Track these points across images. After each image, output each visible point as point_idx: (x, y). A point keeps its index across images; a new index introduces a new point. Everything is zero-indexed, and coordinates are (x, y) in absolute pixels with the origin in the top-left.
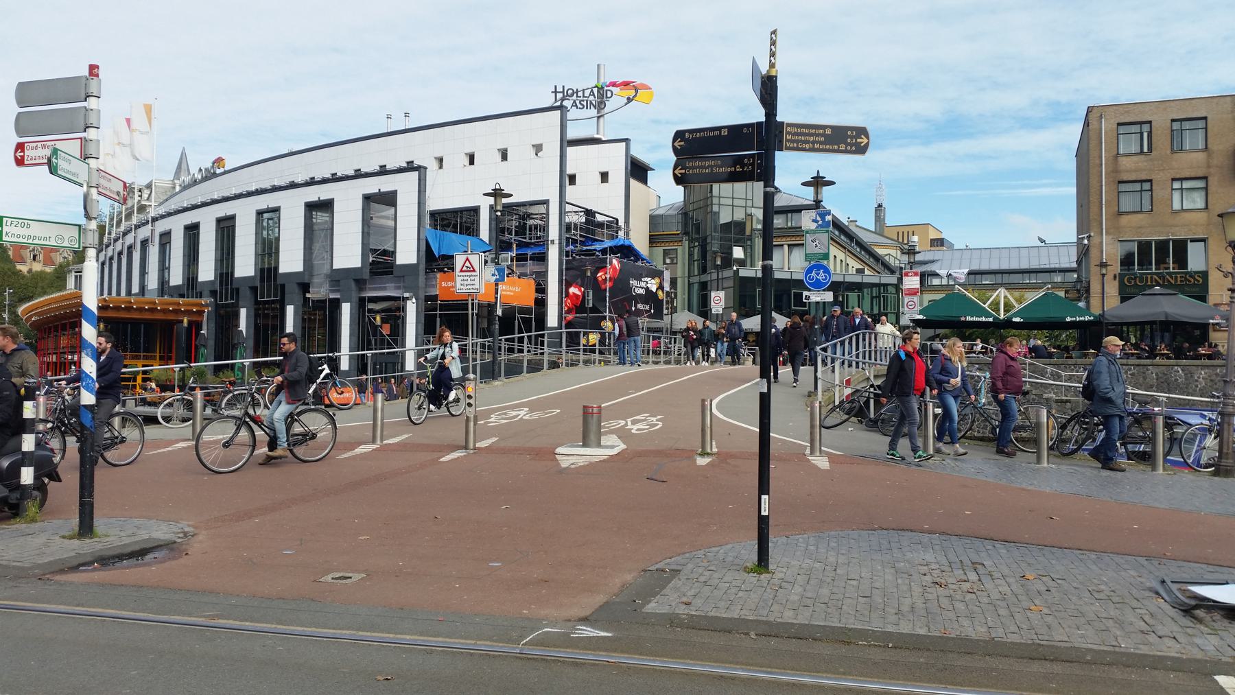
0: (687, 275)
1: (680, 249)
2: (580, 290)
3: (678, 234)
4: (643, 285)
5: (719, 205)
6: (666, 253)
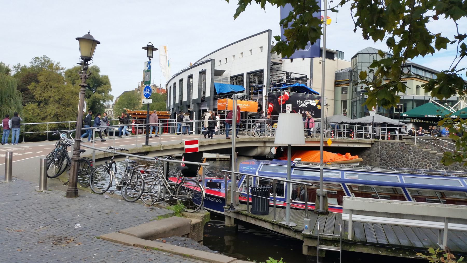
0: (351, 98)
1: (348, 87)
2: (272, 105)
3: (348, 80)
4: (307, 103)
5: (362, 66)
6: (343, 89)
